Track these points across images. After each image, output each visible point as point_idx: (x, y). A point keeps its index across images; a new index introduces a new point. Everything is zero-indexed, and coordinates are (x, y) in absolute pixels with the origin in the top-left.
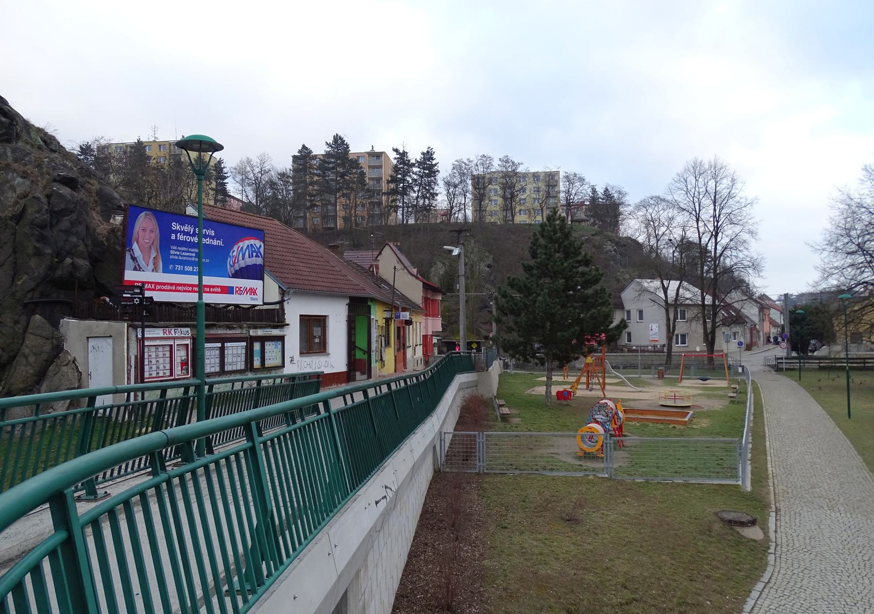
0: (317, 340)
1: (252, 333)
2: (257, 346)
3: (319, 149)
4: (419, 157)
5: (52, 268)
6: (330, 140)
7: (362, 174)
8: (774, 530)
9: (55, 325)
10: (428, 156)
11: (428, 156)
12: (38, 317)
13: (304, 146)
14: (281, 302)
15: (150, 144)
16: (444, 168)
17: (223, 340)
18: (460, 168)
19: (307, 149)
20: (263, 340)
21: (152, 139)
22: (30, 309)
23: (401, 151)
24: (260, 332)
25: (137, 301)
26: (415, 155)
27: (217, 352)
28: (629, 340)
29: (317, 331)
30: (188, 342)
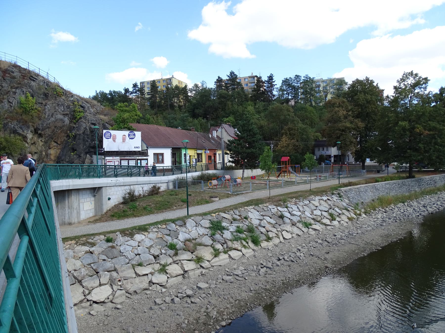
0: (160, 160)
1: (137, 158)
2: (139, 161)
3: (225, 77)
4: (266, 79)
5: (90, 144)
6: (229, 74)
7: (243, 88)
8: (290, 215)
9: (92, 157)
10: (271, 78)
11: (271, 78)
12: (88, 155)
13: (219, 77)
14: (147, 150)
15: (159, 81)
16: (278, 83)
17: (128, 160)
18: (286, 82)
19: (220, 78)
20: (141, 160)
21: (160, 78)
22: (86, 153)
23: (259, 77)
24: (140, 158)
25: (103, 151)
26: (265, 78)
27: (127, 163)
28: (349, 160)
29: (160, 157)
30: (118, 160)
